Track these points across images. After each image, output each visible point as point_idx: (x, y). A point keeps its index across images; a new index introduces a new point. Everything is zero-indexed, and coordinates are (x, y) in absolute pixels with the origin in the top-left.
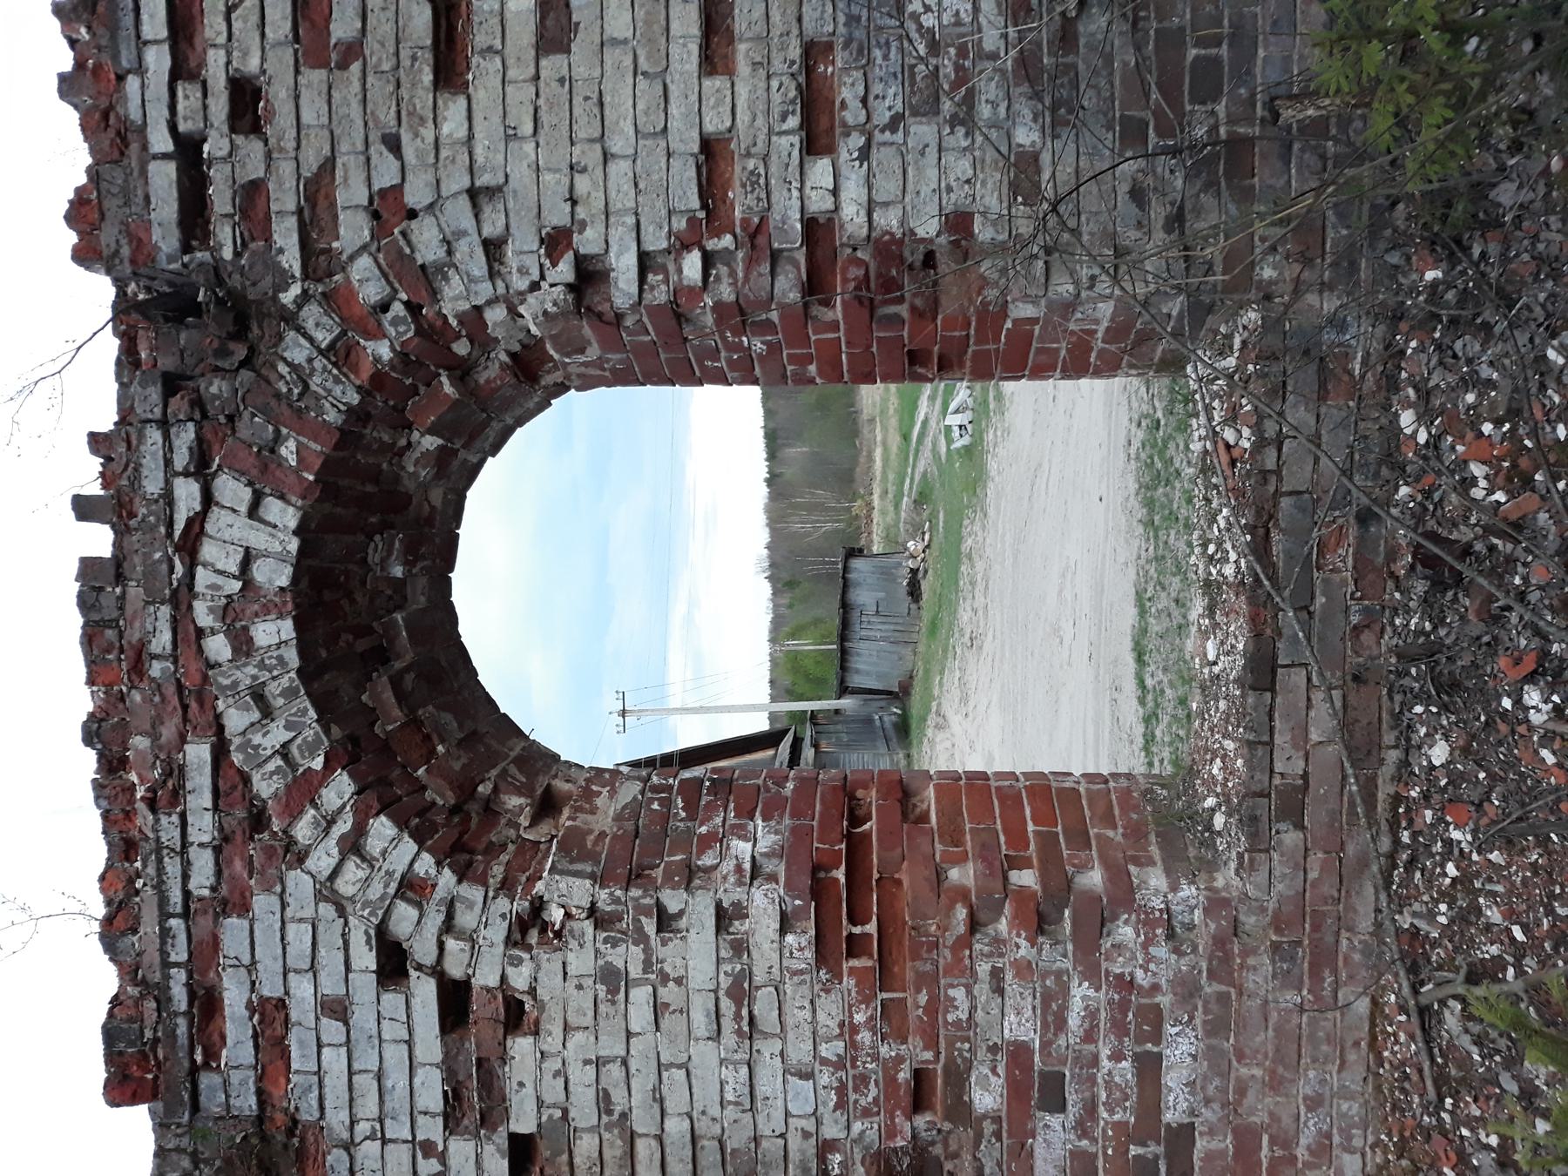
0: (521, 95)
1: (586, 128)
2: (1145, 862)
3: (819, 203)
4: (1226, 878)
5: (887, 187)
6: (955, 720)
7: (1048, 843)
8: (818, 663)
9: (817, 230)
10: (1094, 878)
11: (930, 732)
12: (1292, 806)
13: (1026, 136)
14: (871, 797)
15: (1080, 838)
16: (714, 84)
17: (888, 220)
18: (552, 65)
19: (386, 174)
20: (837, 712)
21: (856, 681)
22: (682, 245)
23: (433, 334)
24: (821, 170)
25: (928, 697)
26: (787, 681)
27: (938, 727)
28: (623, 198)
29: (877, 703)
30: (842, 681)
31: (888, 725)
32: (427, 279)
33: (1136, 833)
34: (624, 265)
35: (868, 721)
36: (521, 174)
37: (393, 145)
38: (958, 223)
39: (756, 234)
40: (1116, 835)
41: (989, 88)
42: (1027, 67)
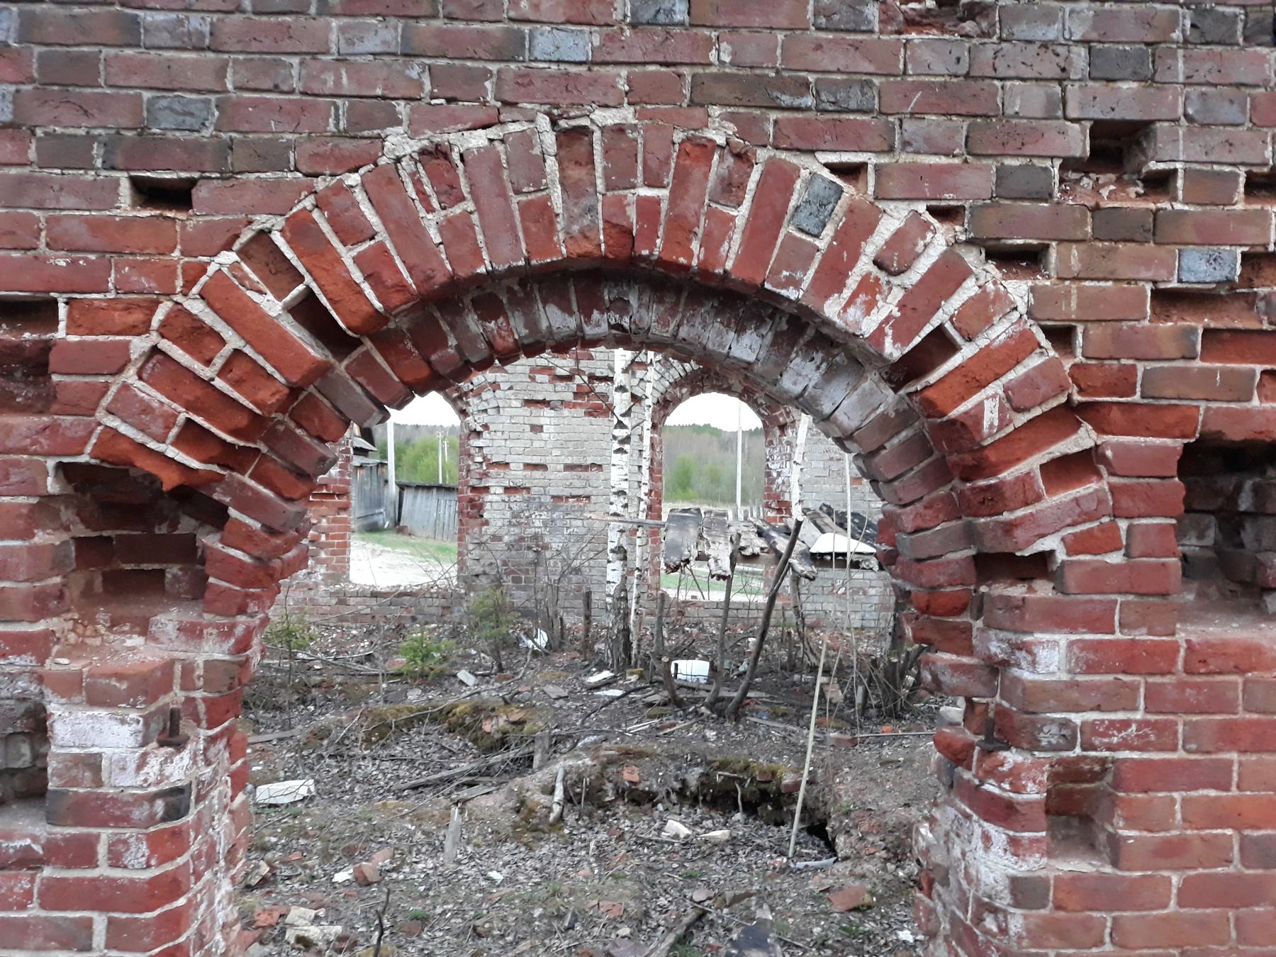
0: (521, 420)
1: (512, 435)
2: (327, 568)
3: (492, 490)
4: (322, 588)
5: (495, 506)
6: (378, 561)
7: (332, 545)
8: (428, 467)
9: (486, 489)
10: (323, 555)
11: (370, 546)
12: (342, 602)
13: (506, 539)
14: (344, 500)
15: (333, 553)
16: (521, 466)
17: (488, 506)
18: (528, 428)
19: (502, 386)
20: (386, 481)
21: (408, 496)
22: (484, 458)
23: (466, 394)
24: (501, 491)
25: (394, 545)
26: (418, 440)
27: (374, 551)
28: (496, 443)
29: (392, 511)
30: (408, 486)
31: (375, 518)
32: (478, 394)
33: (334, 568)
34: (479, 443)
35: (379, 505)
36: (502, 419)
37: (511, 388)
38: (487, 523)
39: (486, 475)
40: (334, 563)
41: (517, 530)
42: (522, 539)
